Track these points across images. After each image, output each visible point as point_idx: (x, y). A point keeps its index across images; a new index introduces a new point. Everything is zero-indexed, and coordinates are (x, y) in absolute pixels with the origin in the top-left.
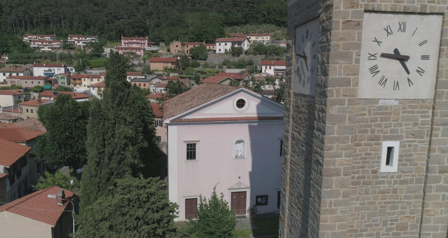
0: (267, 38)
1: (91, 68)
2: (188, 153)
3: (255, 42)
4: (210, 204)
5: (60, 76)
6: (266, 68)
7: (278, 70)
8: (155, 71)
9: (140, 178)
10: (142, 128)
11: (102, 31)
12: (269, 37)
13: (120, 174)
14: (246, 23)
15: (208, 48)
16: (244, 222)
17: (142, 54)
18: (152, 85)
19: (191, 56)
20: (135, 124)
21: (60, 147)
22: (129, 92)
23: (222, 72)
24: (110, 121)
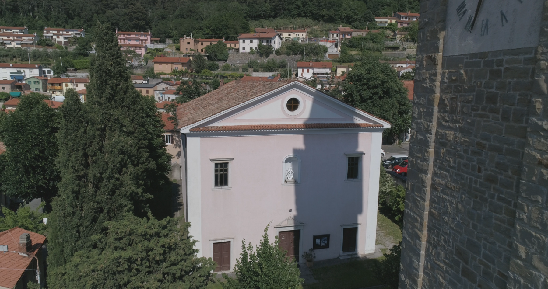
0: (303, 35)
1: (76, 70)
2: (216, 176)
3: (287, 39)
4: (259, 254)
5: (33, 80)
6: (303, 71)
7: (318, 74)
8: (160, 74)
9: (148, 219)
10: (147, 141)
11: (89, 23)
12: (305, 34)
13: (114, 210)
14: (275, 17)
15: (228, 46)
16: (291, 270)
17: (144, 53)
18: (158, 92)
19: (207, 56)
20: (136, 135)
21: (27, 173)
22: (127, 88)
23: (247, 75)
24: (96, 126)
